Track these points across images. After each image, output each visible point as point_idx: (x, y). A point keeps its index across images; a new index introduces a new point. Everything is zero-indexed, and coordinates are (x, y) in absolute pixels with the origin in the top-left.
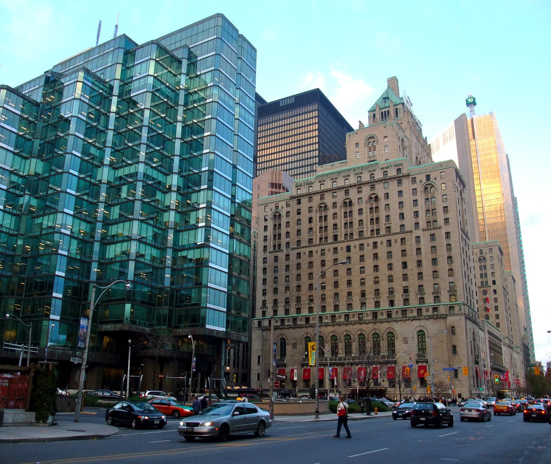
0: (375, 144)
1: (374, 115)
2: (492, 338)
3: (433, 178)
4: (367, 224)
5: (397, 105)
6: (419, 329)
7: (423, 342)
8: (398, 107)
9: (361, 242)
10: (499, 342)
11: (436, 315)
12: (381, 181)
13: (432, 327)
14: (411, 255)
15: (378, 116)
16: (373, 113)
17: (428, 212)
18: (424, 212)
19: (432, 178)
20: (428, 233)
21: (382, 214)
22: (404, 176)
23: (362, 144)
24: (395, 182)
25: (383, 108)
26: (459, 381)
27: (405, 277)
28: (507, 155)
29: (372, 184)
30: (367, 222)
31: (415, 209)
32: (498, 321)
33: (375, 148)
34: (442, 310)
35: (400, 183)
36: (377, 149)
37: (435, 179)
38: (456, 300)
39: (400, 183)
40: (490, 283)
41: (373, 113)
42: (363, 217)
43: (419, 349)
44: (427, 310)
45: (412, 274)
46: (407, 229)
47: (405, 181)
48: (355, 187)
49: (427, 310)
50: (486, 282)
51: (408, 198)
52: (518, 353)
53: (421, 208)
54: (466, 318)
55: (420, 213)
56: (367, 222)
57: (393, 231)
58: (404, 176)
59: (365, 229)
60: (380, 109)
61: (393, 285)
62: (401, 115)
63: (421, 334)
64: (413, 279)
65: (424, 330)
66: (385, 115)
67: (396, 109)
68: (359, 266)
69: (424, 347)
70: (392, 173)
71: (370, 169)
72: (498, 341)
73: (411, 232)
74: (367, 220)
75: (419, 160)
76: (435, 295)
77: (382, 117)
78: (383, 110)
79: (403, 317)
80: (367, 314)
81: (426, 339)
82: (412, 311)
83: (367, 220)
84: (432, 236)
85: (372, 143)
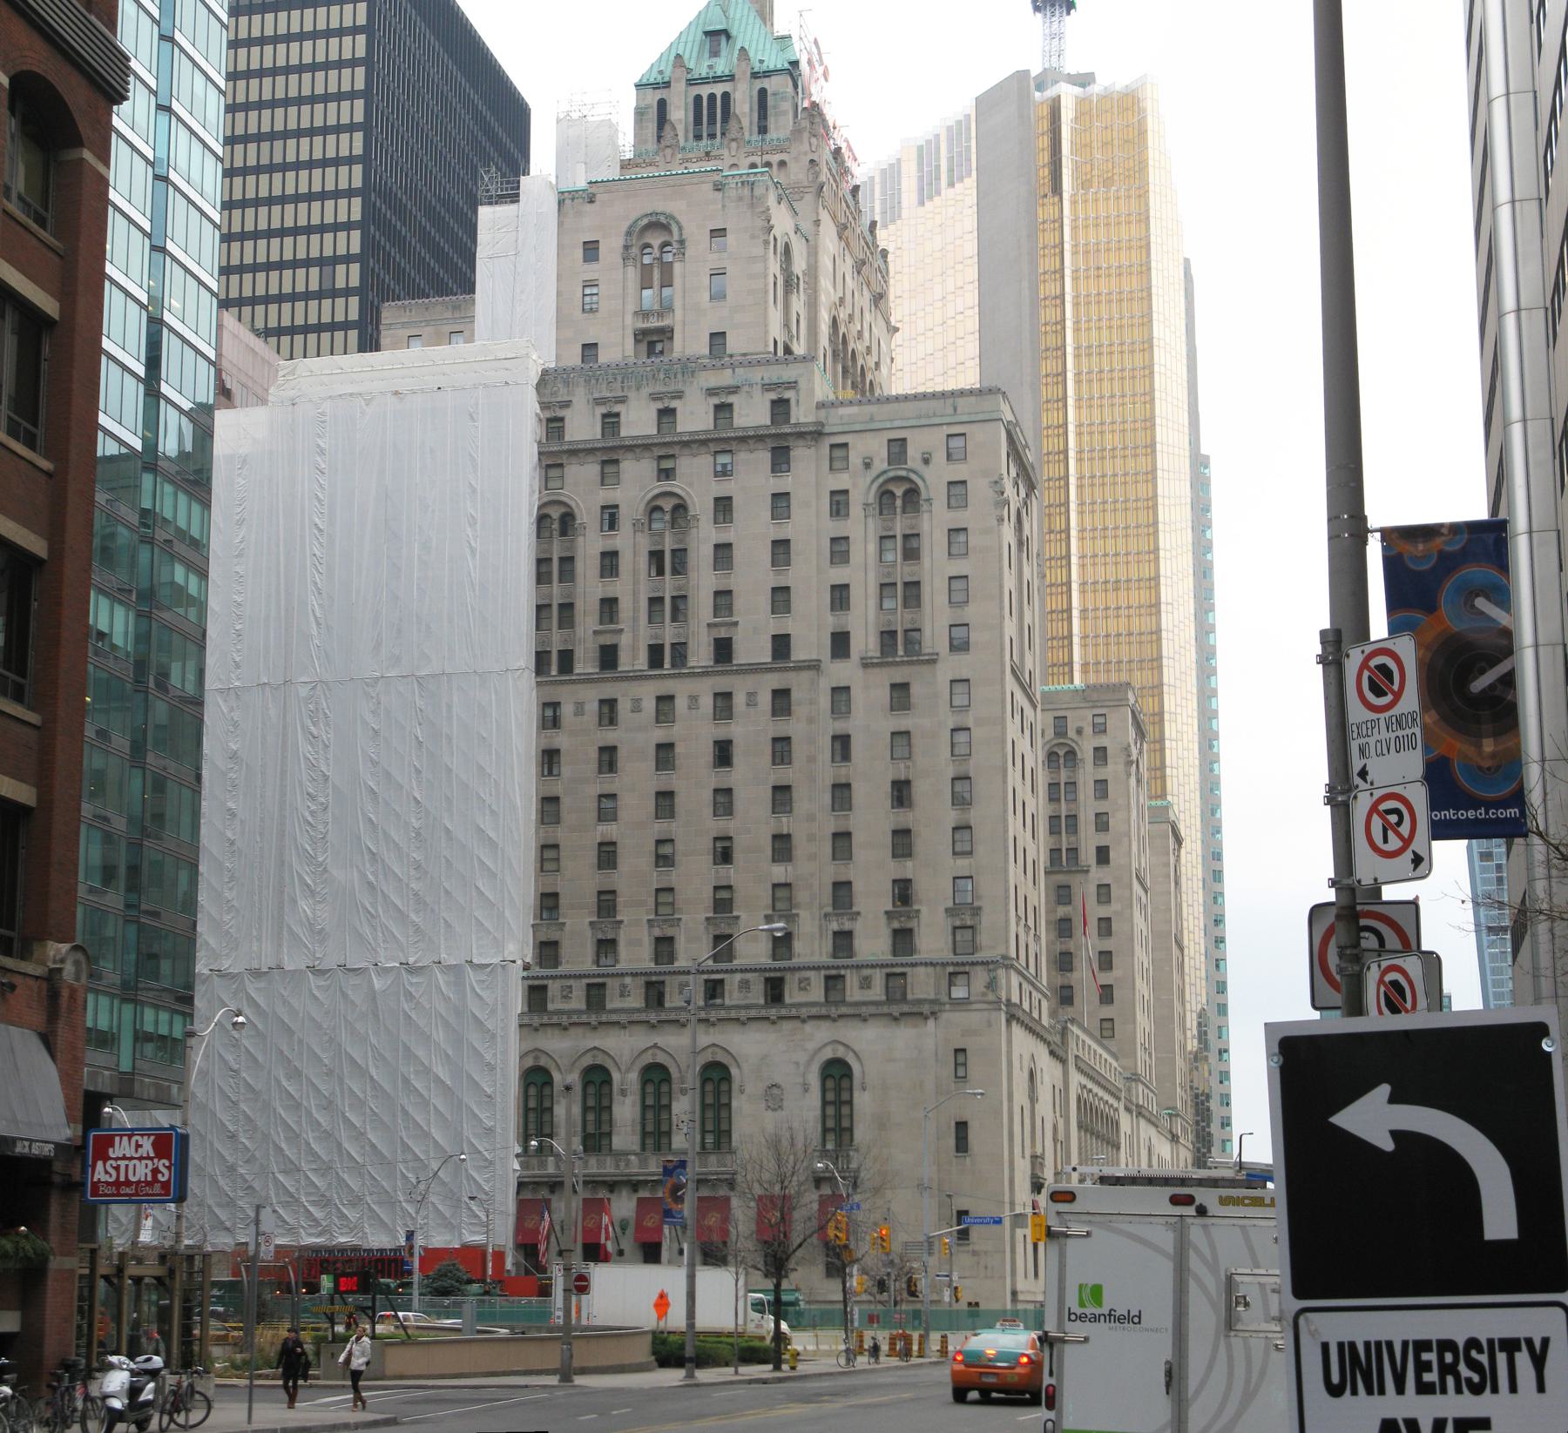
0: (668, 258)
1: (662, 104)
2: (1090, 1085)
3: (919, 456)
4: (635, 619)
5: (768, 74)
6: (828, 1054)
7: (842, 1103)
8: (771, 84)
9: (608, 691)
10: (1111, 1101)
11: (899, 1005)
12: (704, 443)
13: (875, 1047)
14: (811, 759)
15: (679, 114)
16: (659, 95)
17: (887, 591)
18: (873, 589)
19: (913, 454)
20: (882, 680)
21: (703, 581)
22: (801, 435)
23: (611, 247)
24: (764, 457)
25: (705, 81)
26: (975, 1253)
27: (724, 799)
28: (1187, 261)
29: (665, 452)
30: (636, 610)
31: (839, 575)
32: (1107, 1012)
33: (667, 270)
34: (922, 984)
35: (781, 459)
36: (677, 281)
37: (926, 461)
38: (975, 949)
39: (781, 459)
40: (1088, 856)
41: (659, 95)
42: (619, 587)
43: (825, 1130)
44: (866, 983)
45: (811, 838)
46: (799, 653)
47: (805, 458)
48: (590, 458)
49: (866, 983)
50: (1073, 851)
51: (809, 525)
52: (1174, 1139)
53: (862, 575)
54: (1011, 1018)
55: (856, 595)
56: (636, 610)
57: (741, 656)
58: (801, 435)
59: (625, 641)
60: (691, 82)
61: (731, 874)
62: (780, 127)
63: (837, 1074)
64: (812, 857)
65: (851, 1060)
66: (712, 115)
67: (763, 93)
68: (595, 789)
69: (845, 1124)
70: (752, 413)
71: (660, 388)
72: (1107, 1097)
73: (814, 666)
74: (636, 600)
75: (842, 330)
76: (896, 925)
77: (698, 120)
78: (705, 91)
79: (767, 1005)
80: (624, 986)
81: (856, 1094)
82: (804, 985)
83: (636, 600)
84: (900, 691)
85: (656, 253)
